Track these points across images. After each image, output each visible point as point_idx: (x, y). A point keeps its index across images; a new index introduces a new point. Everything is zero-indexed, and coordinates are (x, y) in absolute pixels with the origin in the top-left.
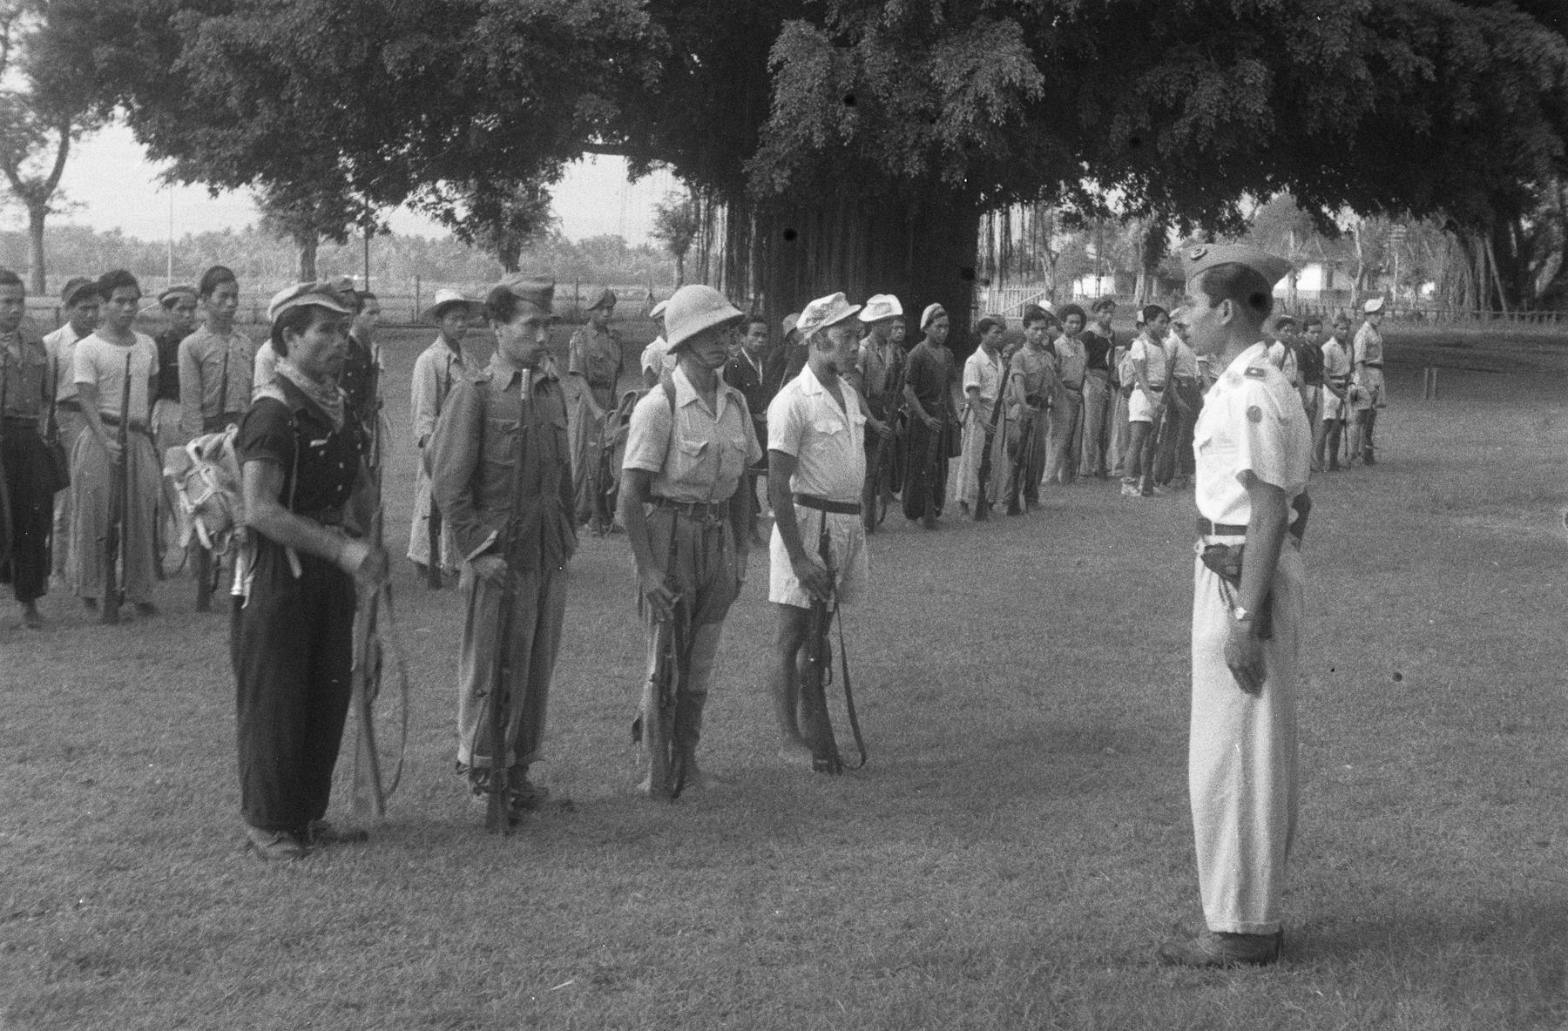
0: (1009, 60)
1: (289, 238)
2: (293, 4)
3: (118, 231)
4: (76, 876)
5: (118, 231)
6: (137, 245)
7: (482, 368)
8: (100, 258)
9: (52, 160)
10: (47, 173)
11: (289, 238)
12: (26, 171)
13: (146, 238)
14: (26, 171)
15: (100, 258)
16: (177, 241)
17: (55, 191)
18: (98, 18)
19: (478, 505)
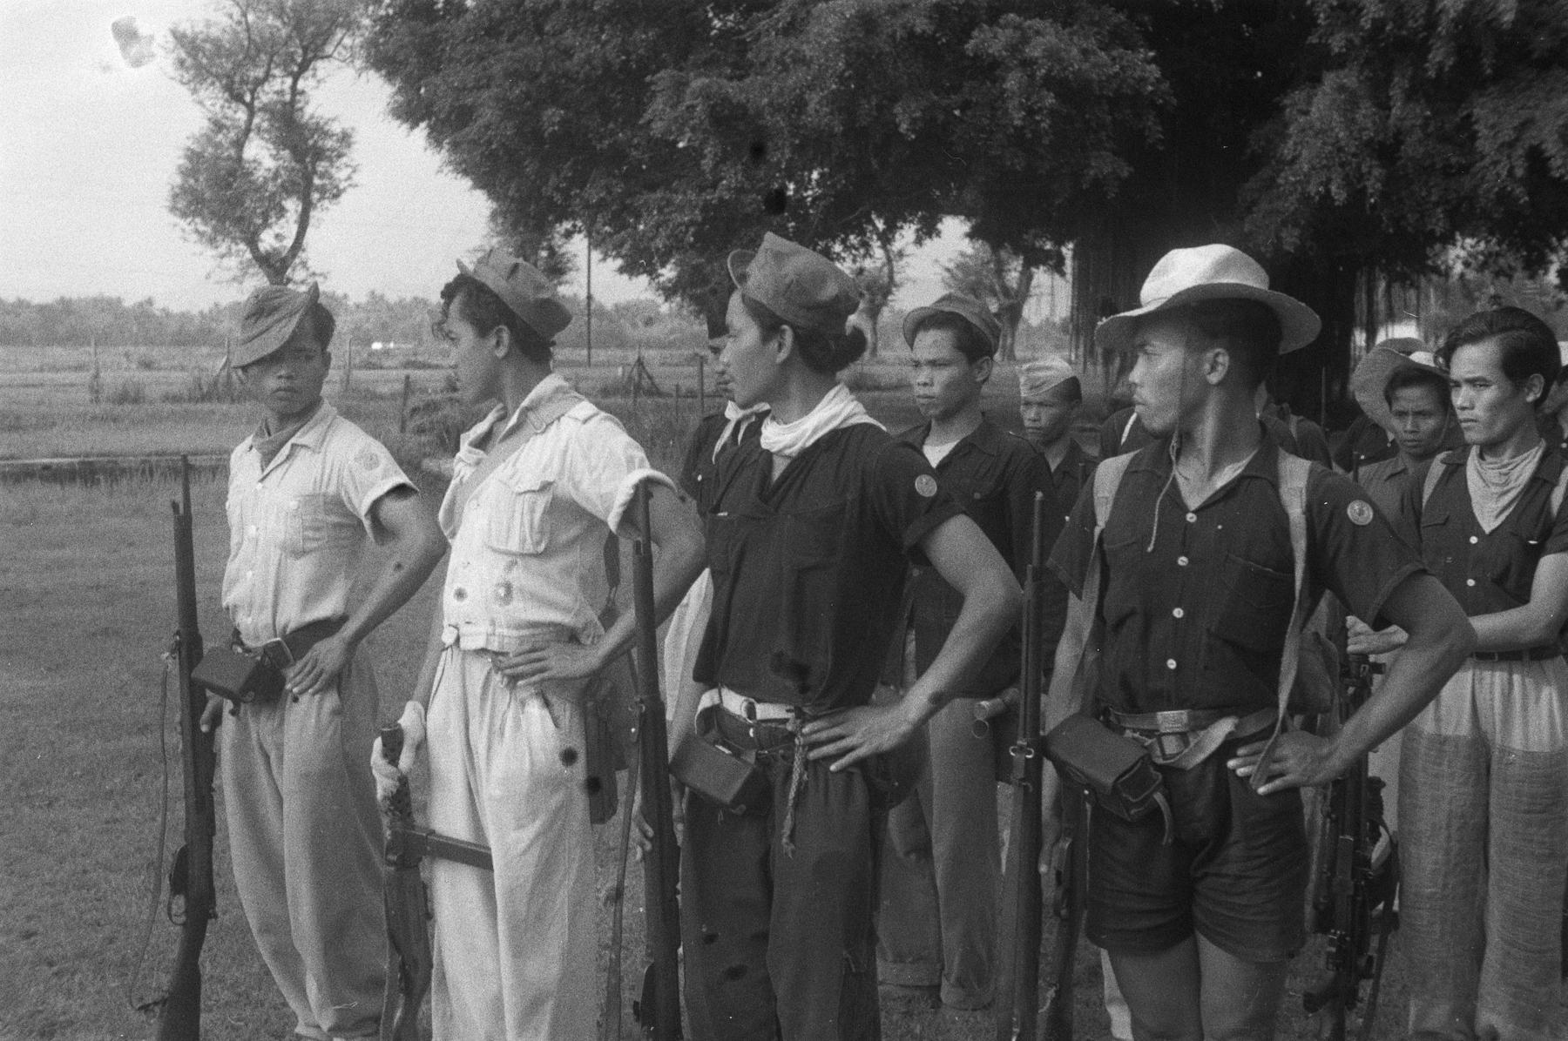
0: (1359, 512)
1: (939, 226)
2: (557, 5)
3: (150, 302)
4: (1392, 121)
5: (150, 302)
6: (168, 315)
7: (743, 296)
8: (135, 329)
9: (294, 229)
10: (289, 243)
11: (939, 226)
12: (267, 241)
13: (175, 309)
14: (267, 241)
15: (135, 329)
16: (206, 311)
17: (297, 261)
18: (543, 80)
19: (809, 309)
